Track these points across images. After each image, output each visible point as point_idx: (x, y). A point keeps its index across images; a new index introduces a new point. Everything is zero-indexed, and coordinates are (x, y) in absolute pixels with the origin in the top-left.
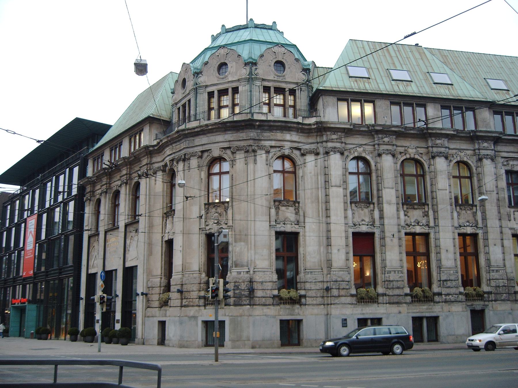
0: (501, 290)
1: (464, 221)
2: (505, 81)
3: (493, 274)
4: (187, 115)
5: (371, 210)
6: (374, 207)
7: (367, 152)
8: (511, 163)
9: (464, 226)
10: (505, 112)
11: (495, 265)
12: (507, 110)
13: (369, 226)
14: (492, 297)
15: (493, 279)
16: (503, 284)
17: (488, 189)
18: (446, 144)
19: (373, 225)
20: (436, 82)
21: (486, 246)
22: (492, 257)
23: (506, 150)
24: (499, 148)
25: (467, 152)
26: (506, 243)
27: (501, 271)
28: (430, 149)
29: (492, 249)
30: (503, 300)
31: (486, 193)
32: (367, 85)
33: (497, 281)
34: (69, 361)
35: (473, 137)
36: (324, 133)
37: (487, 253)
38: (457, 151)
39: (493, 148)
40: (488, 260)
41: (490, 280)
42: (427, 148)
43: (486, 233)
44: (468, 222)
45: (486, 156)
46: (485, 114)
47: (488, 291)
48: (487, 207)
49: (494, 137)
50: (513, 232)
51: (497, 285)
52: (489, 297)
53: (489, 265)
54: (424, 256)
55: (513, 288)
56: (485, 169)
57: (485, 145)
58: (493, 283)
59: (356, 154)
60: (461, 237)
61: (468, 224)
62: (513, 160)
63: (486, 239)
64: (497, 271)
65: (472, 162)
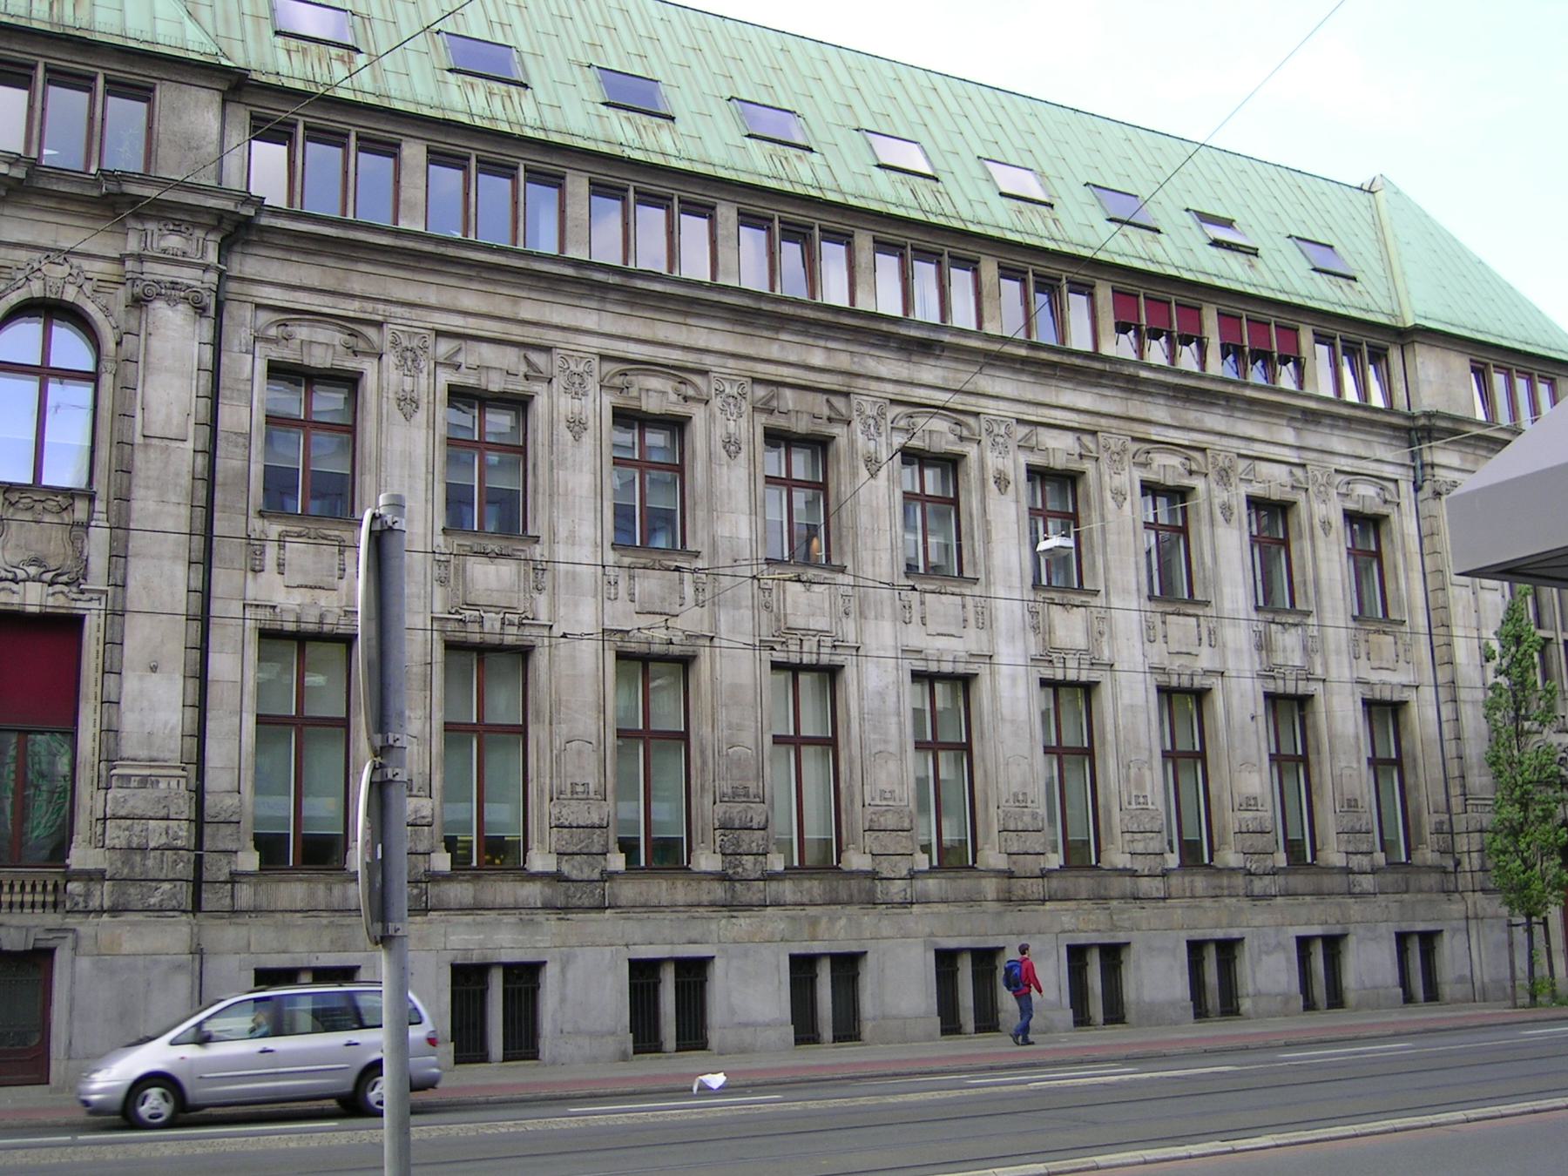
0: (150, 863)
1: (15, 561)
2: (1042, 176)
3: (121, 793)
4: (612, 279)
5: (75, 524)
6: (91, 513)
7: (88, 287)
8: (302, 332)
9: (15, 581)
10: (47, 70)
11: (143, 754)
12: (321, 118)
13: (58, 588)
14: (103, 894)
15: (115, 817)
16: (163, 840)
17: (154, 430)
18: (1288, 435)
19: (77, 580)
20: (884, 161)
21: (111, 669)
22: (130, 722)
23: (283, 278)
24: (248, 265)
25: (86, 264)
26: (222, 664)
27: (163, 785)
28: (129, 265)
29: (132, 683)
30: (160, 910)
31: (146, 446)
32: (340, 71)
33: (138, 826)
34: (1424, 985)
35: (112, 201)
36: (132, 223)
37: (110, 703)
38: (37, 255)
39: (212, 257)
40: (110, 732)
41: (105, 819)
42: (121, 260)
43: (117, 614)
44: (35, 561)
45: (172, 292)
46: (198, 115)
47: (90, 866)
48: (136, 505)
49: (220, 215)
50: (1163, 679)
51: (135, 842)
52: (88, 895)
53: (110, 756)
54: (656, 732)
55: (224, 859)
56: (155, 343)
57: (174, 242)
58: (116, 834)
59: (36, 289)
60: (1051, 690)
61: (33, 571)
62: (646, 372)
63: (113, 642)
64: (144, 781)
65: (106, 310)
